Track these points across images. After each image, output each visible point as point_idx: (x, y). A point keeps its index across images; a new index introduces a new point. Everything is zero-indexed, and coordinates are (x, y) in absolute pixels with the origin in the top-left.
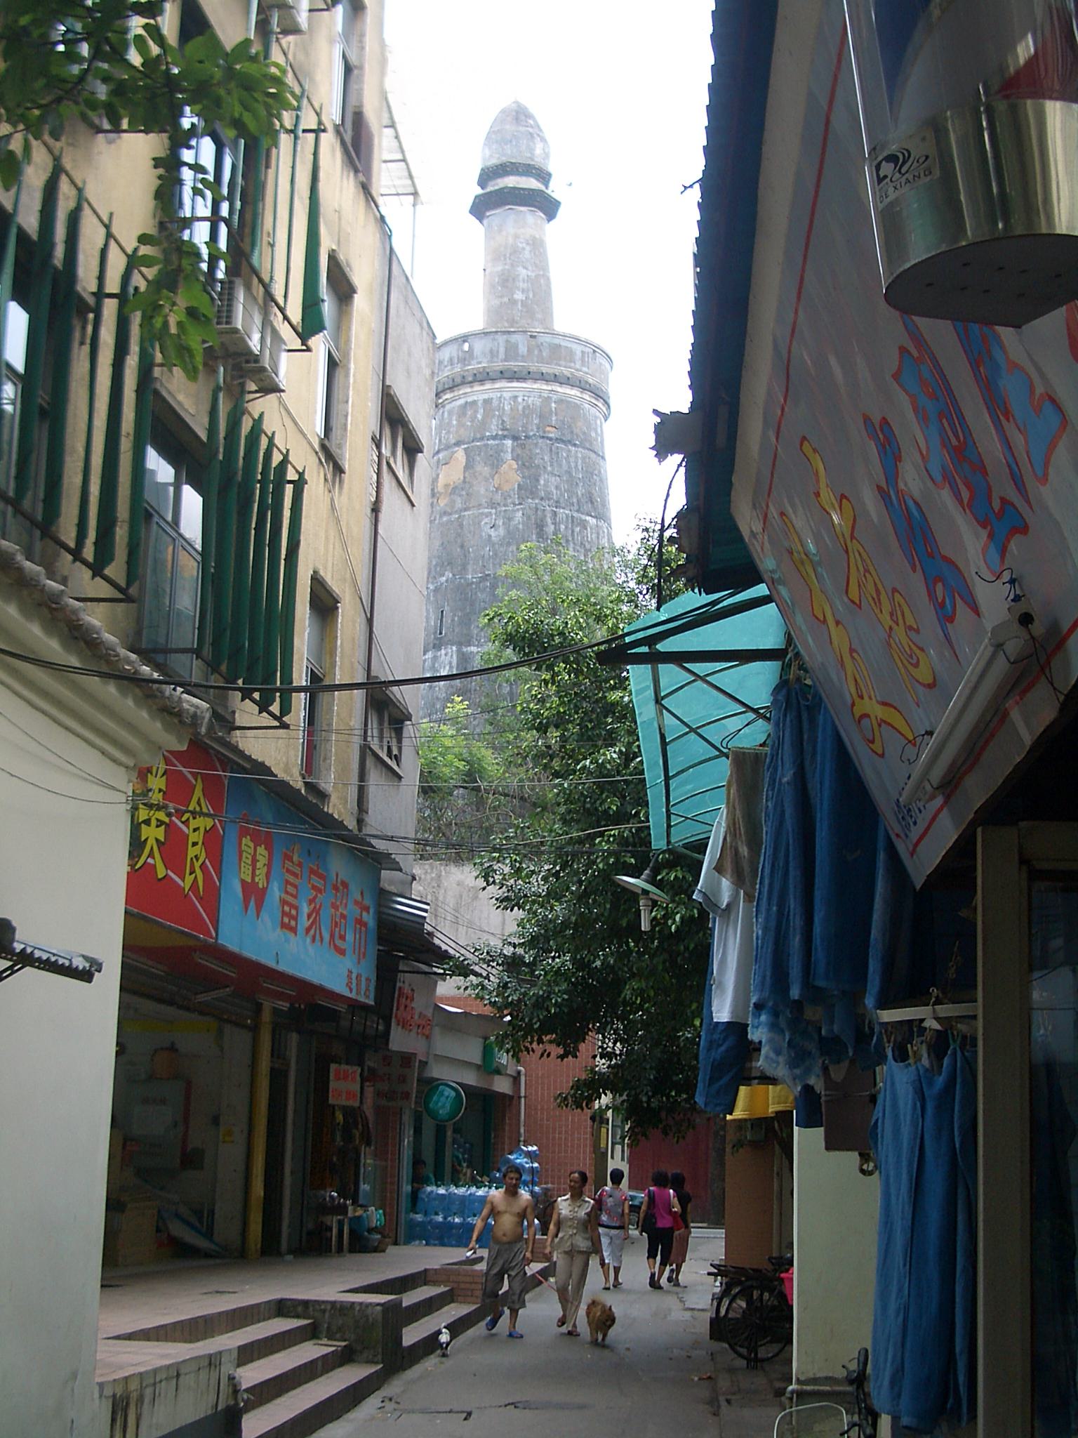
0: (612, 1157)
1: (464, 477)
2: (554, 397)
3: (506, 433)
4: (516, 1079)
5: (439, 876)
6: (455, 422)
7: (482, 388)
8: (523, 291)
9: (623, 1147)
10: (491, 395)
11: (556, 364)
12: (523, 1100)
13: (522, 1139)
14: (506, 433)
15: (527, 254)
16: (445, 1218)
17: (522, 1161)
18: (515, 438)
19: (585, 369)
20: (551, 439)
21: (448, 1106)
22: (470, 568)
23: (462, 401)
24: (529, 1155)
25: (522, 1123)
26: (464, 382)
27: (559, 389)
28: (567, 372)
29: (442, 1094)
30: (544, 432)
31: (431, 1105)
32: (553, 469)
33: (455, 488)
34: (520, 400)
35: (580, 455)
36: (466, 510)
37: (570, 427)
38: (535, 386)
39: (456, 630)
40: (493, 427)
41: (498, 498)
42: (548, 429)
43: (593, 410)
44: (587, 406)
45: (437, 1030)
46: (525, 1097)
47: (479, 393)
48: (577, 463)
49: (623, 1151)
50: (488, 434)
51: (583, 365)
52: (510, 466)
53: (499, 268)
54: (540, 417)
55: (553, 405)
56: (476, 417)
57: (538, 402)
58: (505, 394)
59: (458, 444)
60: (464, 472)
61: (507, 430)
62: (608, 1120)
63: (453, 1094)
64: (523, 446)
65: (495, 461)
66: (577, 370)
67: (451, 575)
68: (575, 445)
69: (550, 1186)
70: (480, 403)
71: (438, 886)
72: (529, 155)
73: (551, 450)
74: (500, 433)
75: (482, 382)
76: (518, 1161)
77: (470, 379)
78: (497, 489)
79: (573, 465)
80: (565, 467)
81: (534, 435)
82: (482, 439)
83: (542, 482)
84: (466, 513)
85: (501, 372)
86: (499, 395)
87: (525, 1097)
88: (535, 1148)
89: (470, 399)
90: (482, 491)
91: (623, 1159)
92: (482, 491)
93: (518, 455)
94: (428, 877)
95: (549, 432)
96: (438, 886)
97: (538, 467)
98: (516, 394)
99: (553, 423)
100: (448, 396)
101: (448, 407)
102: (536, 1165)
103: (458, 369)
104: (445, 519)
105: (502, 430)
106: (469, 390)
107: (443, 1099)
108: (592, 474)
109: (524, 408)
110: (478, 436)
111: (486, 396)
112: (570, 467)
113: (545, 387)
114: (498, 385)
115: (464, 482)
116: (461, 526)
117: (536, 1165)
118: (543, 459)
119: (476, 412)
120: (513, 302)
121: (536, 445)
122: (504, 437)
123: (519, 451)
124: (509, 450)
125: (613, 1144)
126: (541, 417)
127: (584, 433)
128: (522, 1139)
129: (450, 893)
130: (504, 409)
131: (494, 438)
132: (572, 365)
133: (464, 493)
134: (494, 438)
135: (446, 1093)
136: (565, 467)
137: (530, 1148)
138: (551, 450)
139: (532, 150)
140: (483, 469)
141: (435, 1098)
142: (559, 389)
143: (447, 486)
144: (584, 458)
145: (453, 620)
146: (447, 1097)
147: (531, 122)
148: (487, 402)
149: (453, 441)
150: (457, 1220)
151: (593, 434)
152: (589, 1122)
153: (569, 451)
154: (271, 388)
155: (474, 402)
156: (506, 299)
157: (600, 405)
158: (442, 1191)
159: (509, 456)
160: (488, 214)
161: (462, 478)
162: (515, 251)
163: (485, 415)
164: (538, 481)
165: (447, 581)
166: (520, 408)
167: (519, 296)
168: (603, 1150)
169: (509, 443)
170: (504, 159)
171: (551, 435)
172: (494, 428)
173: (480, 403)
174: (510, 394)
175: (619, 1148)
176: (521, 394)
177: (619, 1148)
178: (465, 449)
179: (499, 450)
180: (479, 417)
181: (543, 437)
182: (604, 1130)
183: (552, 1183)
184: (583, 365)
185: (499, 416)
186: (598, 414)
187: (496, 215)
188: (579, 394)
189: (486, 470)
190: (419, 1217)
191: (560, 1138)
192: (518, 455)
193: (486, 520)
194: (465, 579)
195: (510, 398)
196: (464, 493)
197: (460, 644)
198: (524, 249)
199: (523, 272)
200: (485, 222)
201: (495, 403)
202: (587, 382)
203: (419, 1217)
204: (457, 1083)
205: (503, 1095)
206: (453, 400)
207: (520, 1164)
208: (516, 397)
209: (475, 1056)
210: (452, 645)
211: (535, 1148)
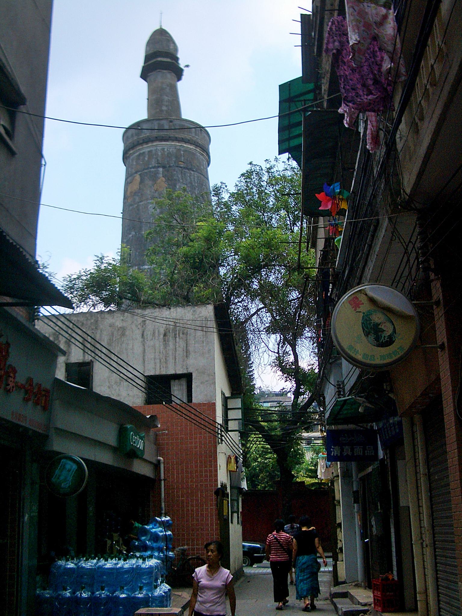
0: (232, 523)
1: (140, 187)
2: (182, 149)
3: (159, 165)
4: (156, 466)
5: (97, 321)
6: (135, 163)
7: (147, 146)
8: (166, 106)
9: (238, 514)
10: (152, 149)
11: (183, 134)
12: (163, 482)
13: (163, 512)
14: (159, 165)
15: (168, 90)
16: (74, 593)
17: (158, 530)
18: (164, 167)
19: (197, 137)
20: (181, 167)
21: (70, 478)
22: (143, 229)
23: (138, 153)
24: (162, 524)
25: (163, 500)
26: (139, 144)
27: (185, 145)
28: (188, 137)
29: (64, 467)
30: (178, 164)
31: (54, 480)
32: (183, 181)
33: (135, 193)
34: (166, 150)
35: (196, 176)
36: (141, 202)
37: (190, 162)
38: (173, 143)
39: (138, 259)
40: (153, 163)
41: (156, 195)
42: (180, 163)
43: (201, 157)
44: (198, 154)
45: (57, 404)
46: (164, 480)
47: (146, 148)
48: (194, 178)
49: (238, 517)
50: (150, 166)
51: (196, 135)
52: (162, 180)
53: (154, 97)
54: (176, 157)
55: (182, 152)
56: (145, 159)
57: (175, 151)
58: (158, 148)
59: (136, 173)
60: (140, 184)
61: (160, 163)
62: (228, 494)
63: (75, 467)
64: (168, 171)
65: (154, 178)
66: (193, 137)
67: (134, 233)
68: (193, 171)
69: (186, 547)
70: (146, 153)
71: (96, 328)
72: (167, 49)
73: (182, 172)
74: (156, 165)
75: (147, 143)
76: (154, 530)
77: (141, 142)
78: (156, 191)
79: (193, 179)
80: (189, 180)
81: (174, 166)
82: (148, 168)
83: (178, 187)
84: (141, 203)
85: (156, 137)
86: (155, 148)
87: (164, 480)
88: (168, 518)
89: (141, 152)
90: (148, 192)
91: (238, 523)
92: (148, 192)
93: (166, 175)
94: (89, 322)
95: (181, 164)
96: (96, 328)
97: (175, 180)
98: (164, 147)
99: (182, 160)
100: (131, 152)
101: (131, 158)
102: (169, 533)
103: (135, 138)
104: (131, 208)
105: (157, 164)
106: (141, 147)
107: (65, 473)
108: (202, 185)
109: (168, 153)
110: (146, 167)
111: (149, 149)
112: (191, 181)
113: (178, 144)
114: (155, 144)
115: (140, 189)
116: (138, 210)
117: (169, 533)
118: (178, 176)
119: (145, 157)
120: (162, 111)
121: (174, 170)
122: (159, 167)
123: (166, 173)
124: (161, 173)
125: (232, 513)
126: (176, 157)
127: (198, 166)
128: (163, 512)
129: (105, 333)
130: (158, 154)
131: (154, 167)
132: (191, 134)
133: (140, 194)
134: (154, 167)
135: (68, 467)
136: (189, 180)
137: (164, 519)
138: (182, 172)
139: (168, 46)
140: (148, 182)
141: (57, 472)
142: (185, 145)
143: (131, 192)
144: (198, 177)
145: (136, 254)
146: (69, 471)
147: (168, 35)
148: (150, 152)
149: (134, 172)
150: (84, 595)
151: (202, 167)
152: (214, 497)
153: (191, 173)
154: (235, 568)
155: (144, 153)
156: (158, 110)
157: (205, 155)
158: (71, 565)
159: (161, 175)
160: (149, 74)
161: (138, 188)
162: (162, 89)
163: (149, 158)
164: (176, 186)
165: (132, 236)
166: (166, 153)
167: (164, 108)
168: (225, 517)
169: (161, 169)
170: (155, 50)
171: (182, 166)
172: (153, 163)
173: (146, 153)
174: (161, 148)
175: (235, 515)
176: (166, 147)
177: (235, 515)
178: (140, 175)
179: (157, 173)
180: (146, 159)
181: (177, 167)
182: (225, 502)
183: (188, 545)
184: (196, 135)
185: (156, 158)
186: (204, 159)
187: (152, 75)
188: (194, 148)
189: (150, 183)
190: (47, 594)
191: (192, 510)
192: (166, 175)
193: (151, 206)
194: (141, 234)
195: (161, 149)
196: (140, 194)
197: (139, 265)
198: (166, 88)
199: (166, 98)
200: (148, 79)
201: (154, 152)
202: (198, 143)
203: (47, 594)
204: (84, 460)
205: (144, 478)
206: (134, 153)
207: (155, 532)
208: (164, 149)
209: (112, 439)
210: (136, 266)
211: (168, 518)
